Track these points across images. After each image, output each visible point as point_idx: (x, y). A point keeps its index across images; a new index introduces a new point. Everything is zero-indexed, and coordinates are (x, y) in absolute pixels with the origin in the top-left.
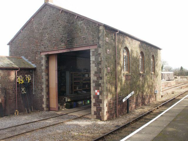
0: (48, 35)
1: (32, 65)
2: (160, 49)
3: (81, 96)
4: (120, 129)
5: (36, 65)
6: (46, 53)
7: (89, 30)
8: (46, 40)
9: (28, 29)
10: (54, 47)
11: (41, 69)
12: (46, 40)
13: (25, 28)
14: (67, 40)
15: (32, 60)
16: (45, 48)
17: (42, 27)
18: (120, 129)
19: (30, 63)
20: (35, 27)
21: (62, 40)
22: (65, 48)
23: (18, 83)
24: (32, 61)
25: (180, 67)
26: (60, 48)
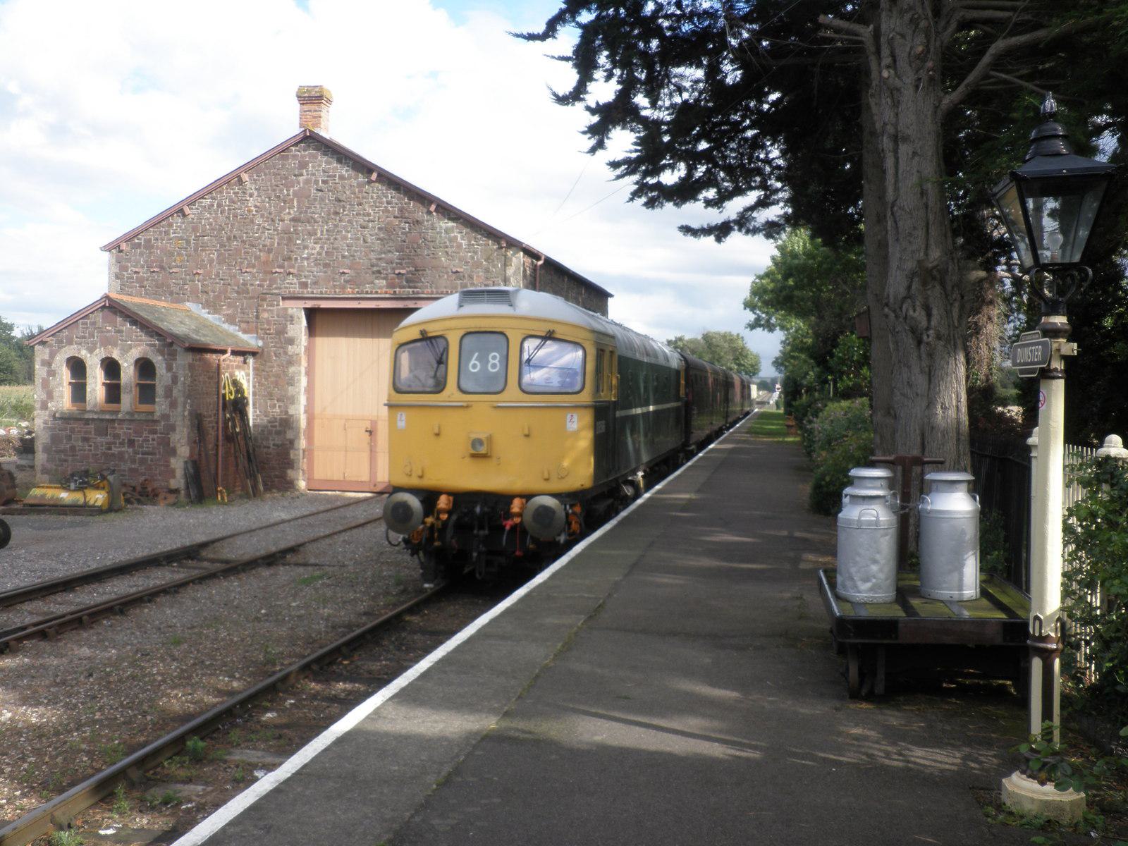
0: (318, 246)
1: (245, 337)
2: (611, 296)
3: (891, 346)
4: (344, 650)
5: (262, 339)
6: (309, 304)
7: (475, 252)
8: (307, 259)
9: (219, 205)
10: (343, 288)
11: (286, 353)
12: (307, 259)
13: (206, 202)
14: (397, 272)
15: (239, 321)
16: (304, 285)
17: (289, 213)
18: (369, 637)
19: (232, 329)
20: (256, 206)
21: (375, 269)
22: (387, 296)
23: (224, 396)
24: (243, 325)
25: (106, 256)
26: (367, 293)
